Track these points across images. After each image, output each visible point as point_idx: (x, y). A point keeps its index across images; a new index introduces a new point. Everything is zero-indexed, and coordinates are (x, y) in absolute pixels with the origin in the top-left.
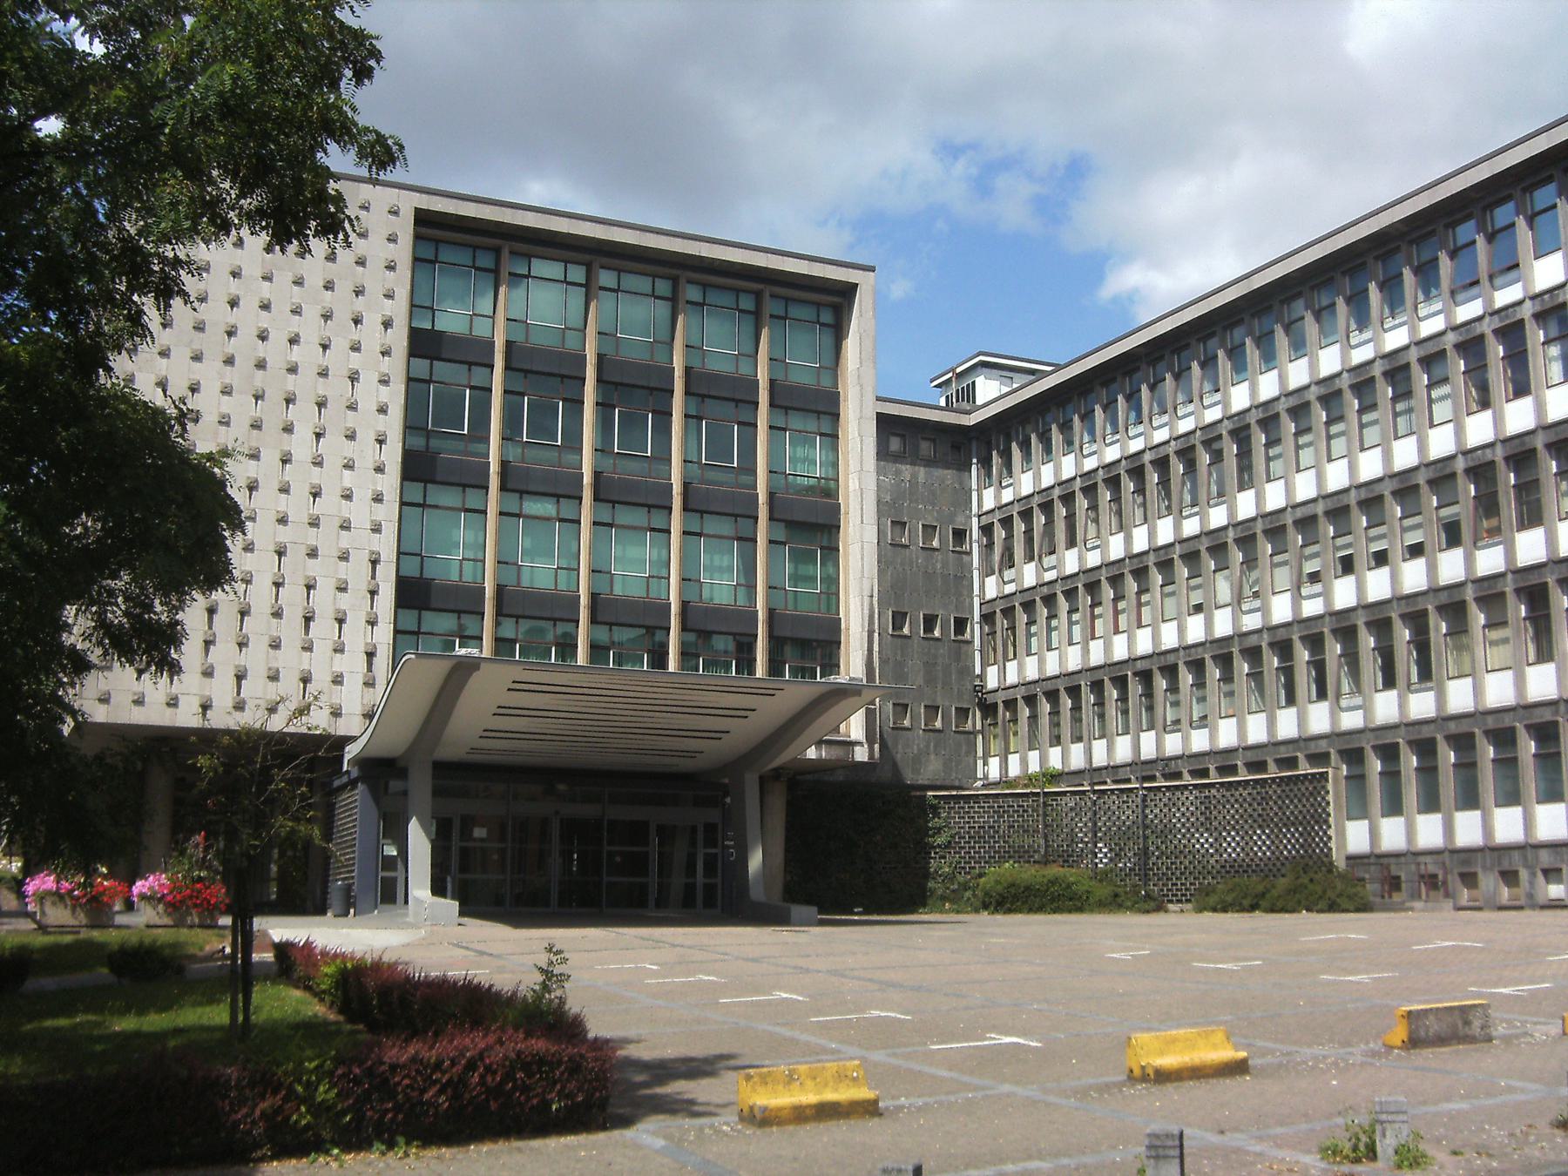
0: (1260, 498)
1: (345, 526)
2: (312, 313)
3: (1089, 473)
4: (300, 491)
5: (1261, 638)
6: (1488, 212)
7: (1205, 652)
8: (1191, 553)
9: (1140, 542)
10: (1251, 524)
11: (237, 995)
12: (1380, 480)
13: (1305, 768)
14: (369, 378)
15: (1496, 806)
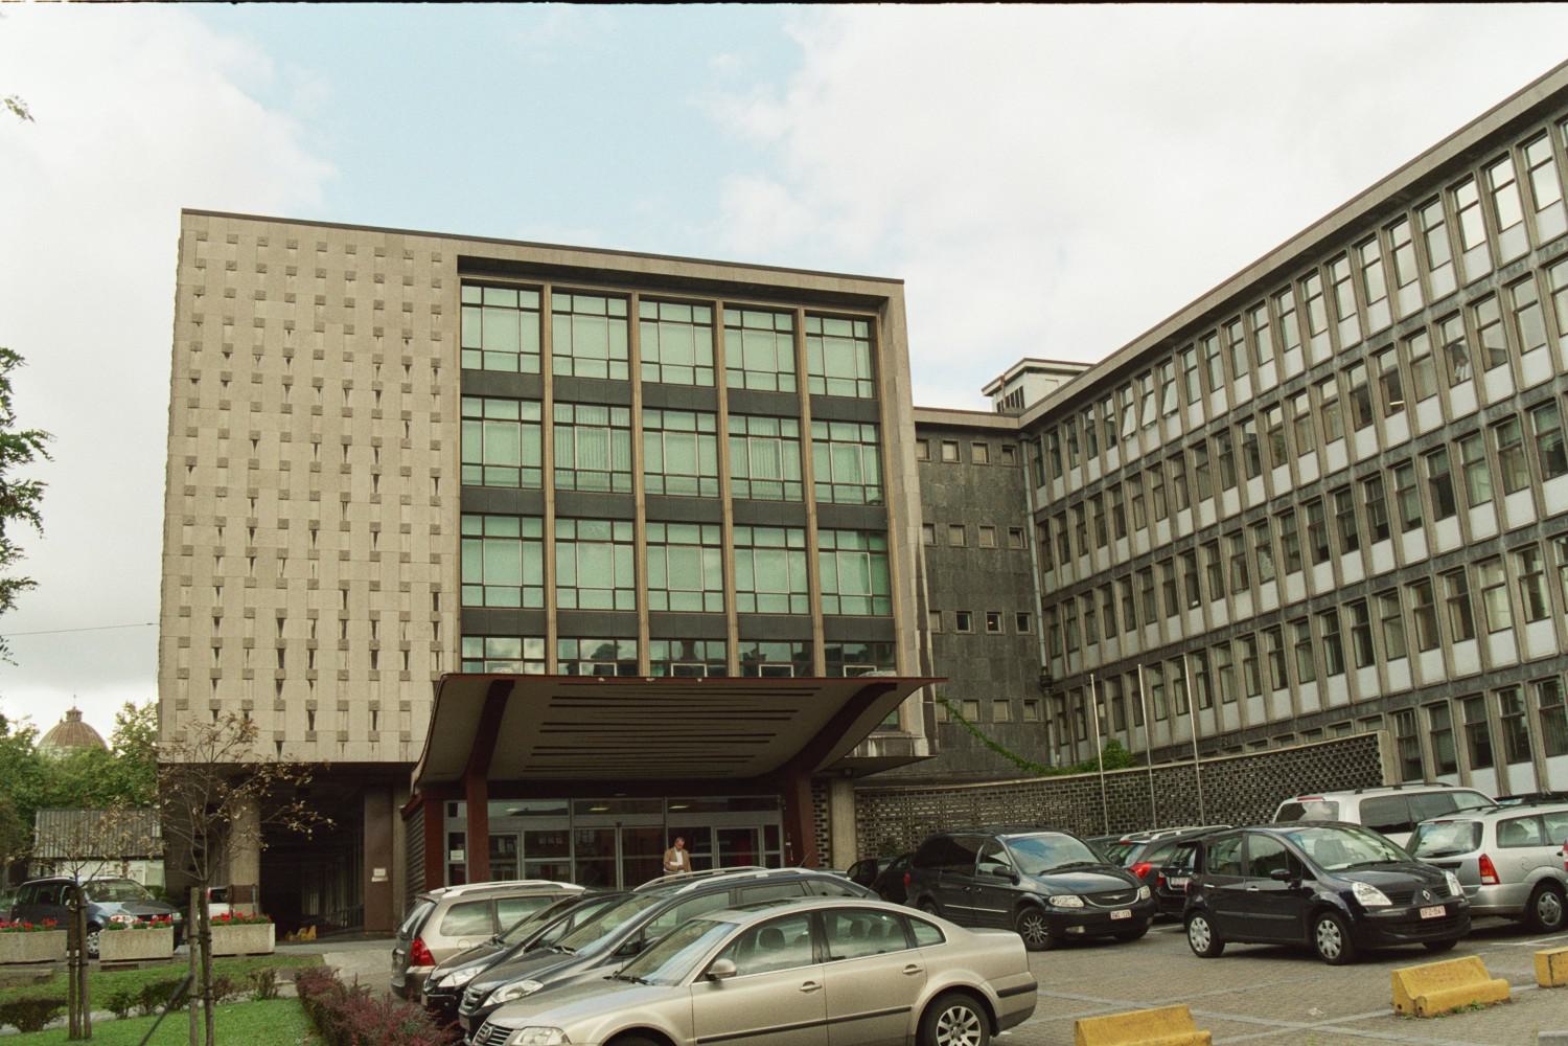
0: (1294, 473)
1: (405, 558)
2: (363, 361)
3: (1132, 463)
4: (361, 530)
5: (1306, 609)
6: (1487, 172)
7: (1253, 627)
8: (1078, 504)
9: (1185, 526)
10: (1288, 498)
11: (489, 1007)
12: (1407, 443)
13: (1362, 731)
14: (420, 421)
15: (1548, 756)
